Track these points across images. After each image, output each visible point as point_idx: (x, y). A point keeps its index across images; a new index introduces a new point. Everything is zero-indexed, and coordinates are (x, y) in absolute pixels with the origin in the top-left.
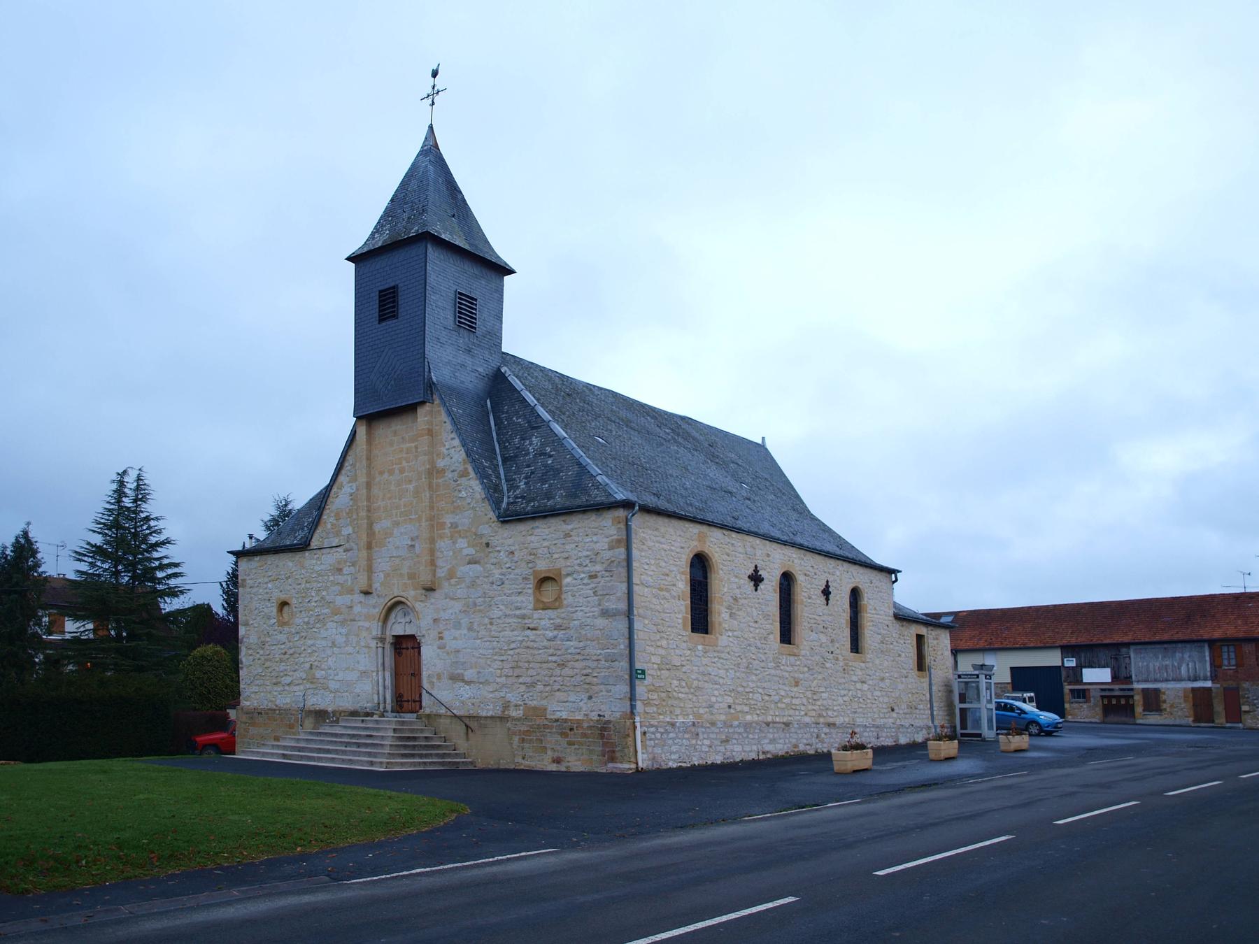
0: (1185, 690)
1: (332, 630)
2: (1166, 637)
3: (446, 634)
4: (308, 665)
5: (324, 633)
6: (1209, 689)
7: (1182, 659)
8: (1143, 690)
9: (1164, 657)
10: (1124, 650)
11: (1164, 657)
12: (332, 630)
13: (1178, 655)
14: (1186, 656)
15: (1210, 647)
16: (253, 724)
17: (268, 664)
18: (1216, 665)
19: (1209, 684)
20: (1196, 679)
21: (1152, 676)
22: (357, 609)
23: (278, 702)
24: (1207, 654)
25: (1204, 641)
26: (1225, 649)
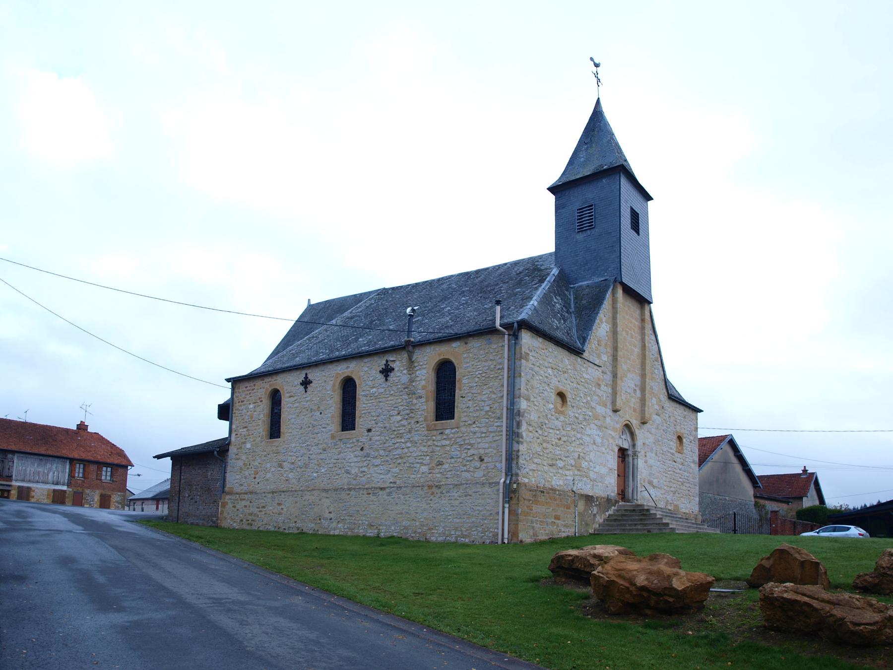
0: (49, 490)
1: (592, 430)
2: (42, 451)
3: (648, 454)
4: (576, 455)
5: (588, 432)
6: (64, 491)
7: (50, 469)
8: (19, 487)
9: (38, 465)
10: (10, 456)
11: (38, 465)
12: (592, 430)
13: (49, 466)
14: (54, 467)
15: (71, 464)
16: (536, 502)
17: (545, 445)
18: (71, 475)
19: (65, 488)
20: (57, 484)
21: (27, 478)
22: (608, 420)
23: (553, 483)
24: (68, 467)
25: (67, 458)
26: (104, 469)
